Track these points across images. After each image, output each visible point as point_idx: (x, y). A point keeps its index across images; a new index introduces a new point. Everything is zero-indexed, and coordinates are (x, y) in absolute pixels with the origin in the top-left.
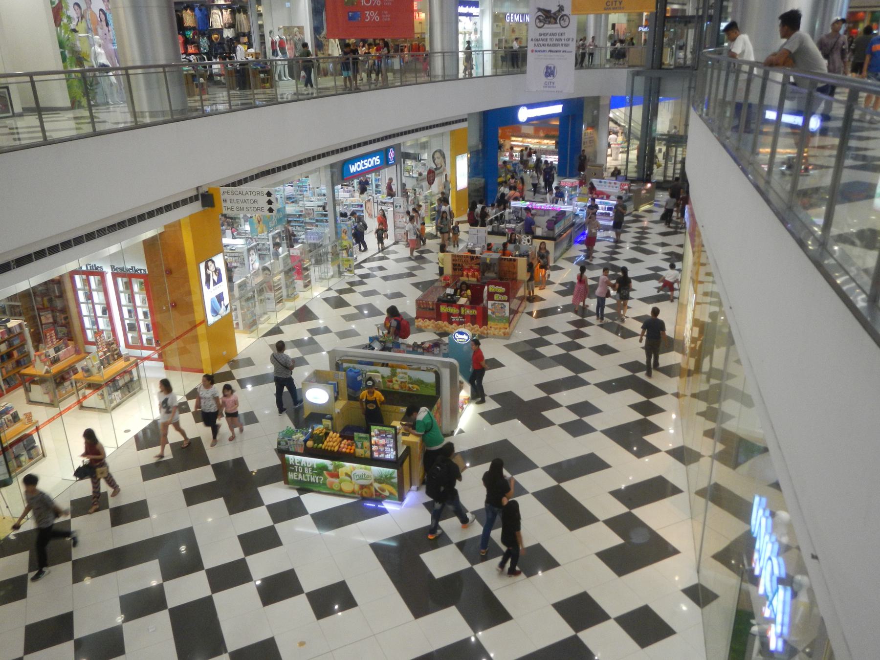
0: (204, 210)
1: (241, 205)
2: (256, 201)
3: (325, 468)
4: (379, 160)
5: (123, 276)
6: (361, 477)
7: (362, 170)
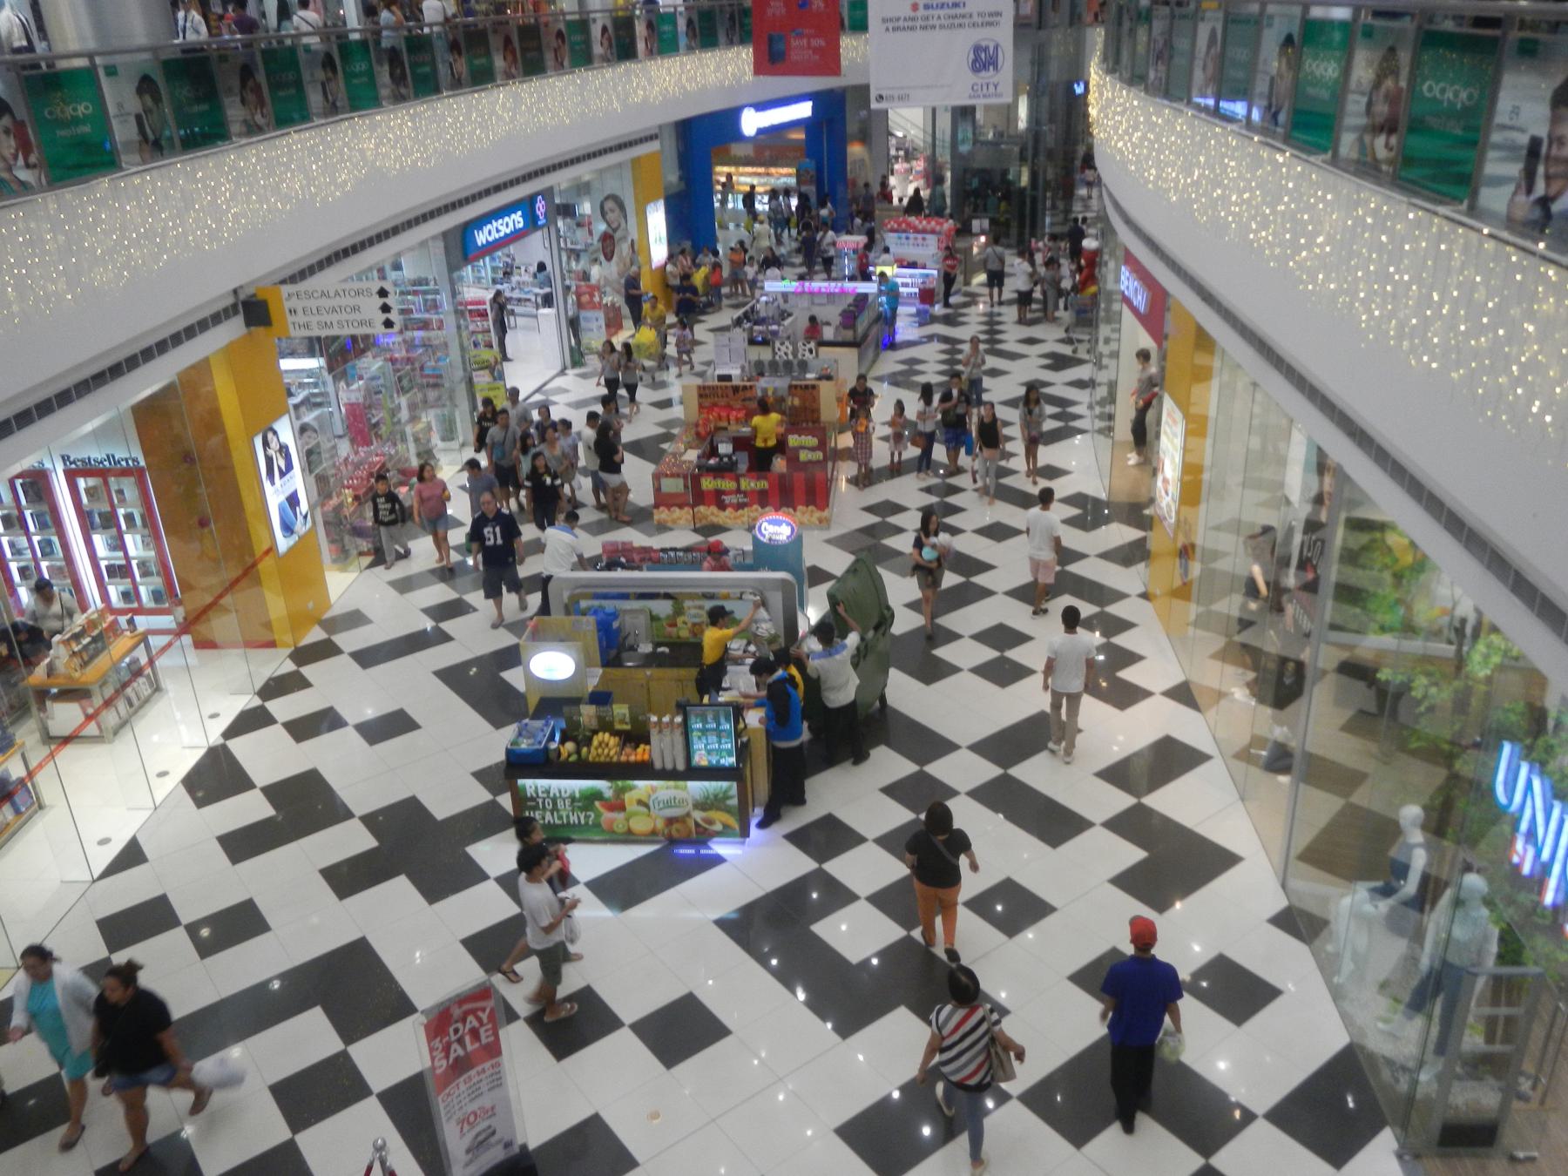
0: (250, 334)
1: (327, 318)
2: (355, 309)
3: (596, 795)
4: (521, 220)
5: (87, 472)
6: (669, 804)
7: (496, 240)
